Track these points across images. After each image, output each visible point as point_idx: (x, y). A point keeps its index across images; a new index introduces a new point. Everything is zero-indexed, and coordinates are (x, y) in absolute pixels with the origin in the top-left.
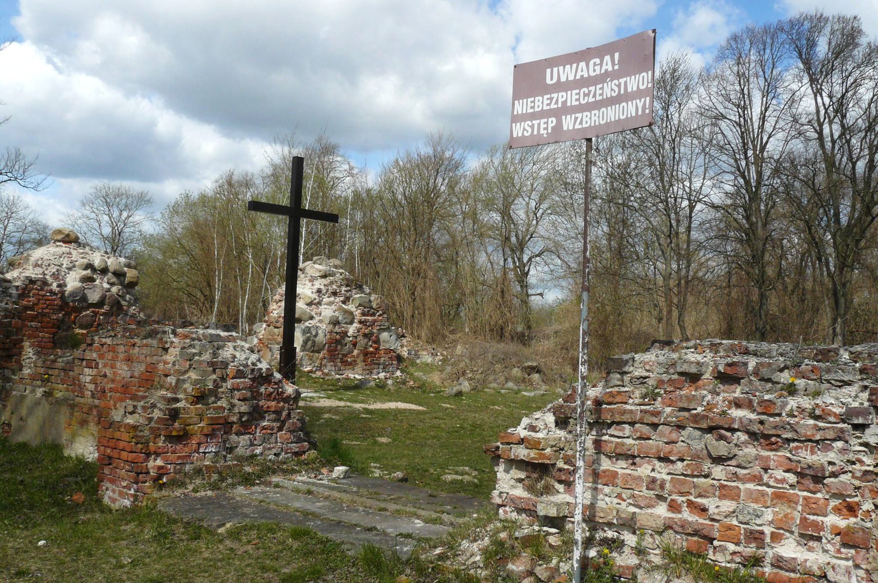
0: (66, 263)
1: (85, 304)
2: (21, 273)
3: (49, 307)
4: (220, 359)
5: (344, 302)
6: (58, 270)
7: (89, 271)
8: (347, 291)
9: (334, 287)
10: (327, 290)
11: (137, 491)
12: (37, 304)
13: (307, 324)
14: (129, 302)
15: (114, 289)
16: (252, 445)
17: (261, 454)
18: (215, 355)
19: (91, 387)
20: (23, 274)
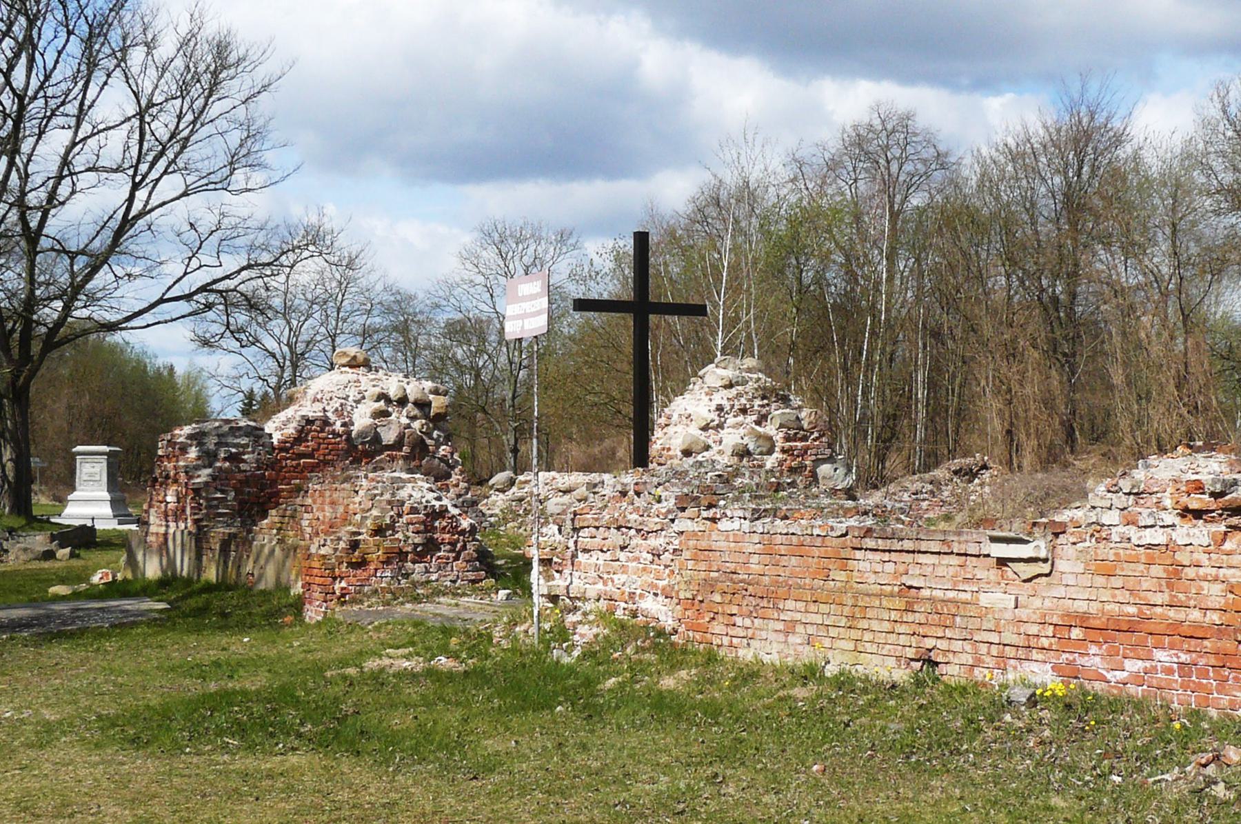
0: (353, 394)
1: (378, 447)
2: (296, 411)
3: (333, 453)
4: (398, 498)
5: (758, 423)
6: (342, 405)
7: (382, 403)
8: (763, 406)
9: (743, 401)
10: (733, 406)
11: (326, 608)
12: (318, 450)
13: (699, 458)
14: (437, 440)
15: (417, 425)
16: (427, 571)
17: (437, 580)
18: (393, 495)
19: (309, 530)
20: (300, 413)
